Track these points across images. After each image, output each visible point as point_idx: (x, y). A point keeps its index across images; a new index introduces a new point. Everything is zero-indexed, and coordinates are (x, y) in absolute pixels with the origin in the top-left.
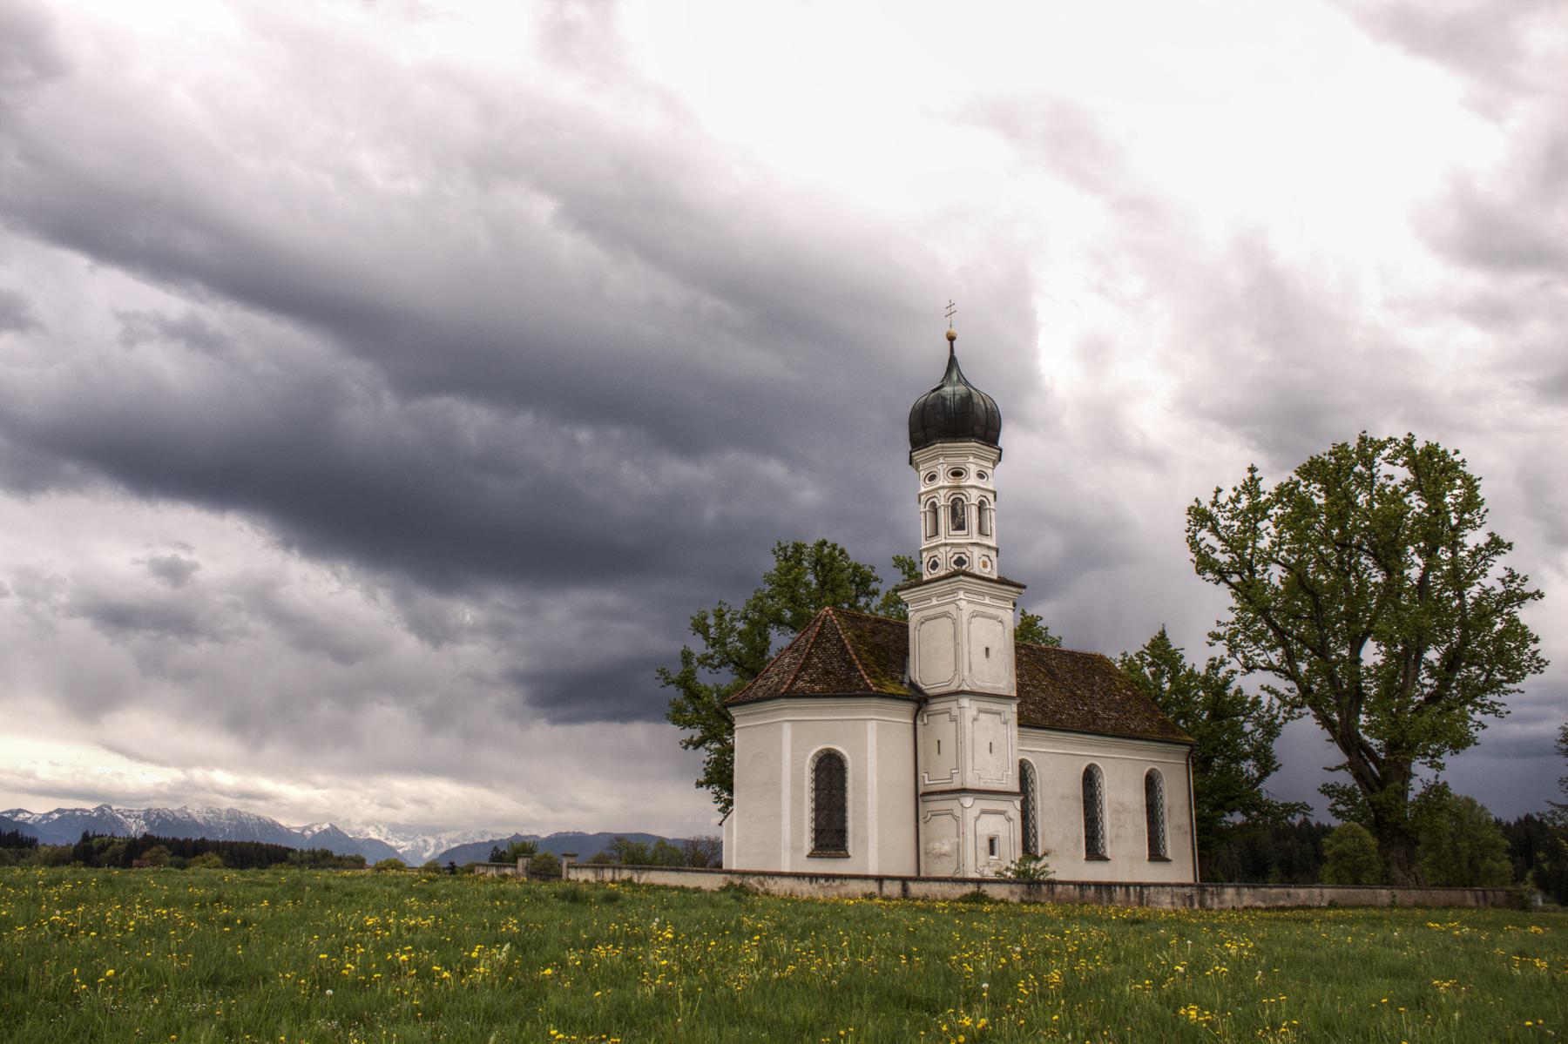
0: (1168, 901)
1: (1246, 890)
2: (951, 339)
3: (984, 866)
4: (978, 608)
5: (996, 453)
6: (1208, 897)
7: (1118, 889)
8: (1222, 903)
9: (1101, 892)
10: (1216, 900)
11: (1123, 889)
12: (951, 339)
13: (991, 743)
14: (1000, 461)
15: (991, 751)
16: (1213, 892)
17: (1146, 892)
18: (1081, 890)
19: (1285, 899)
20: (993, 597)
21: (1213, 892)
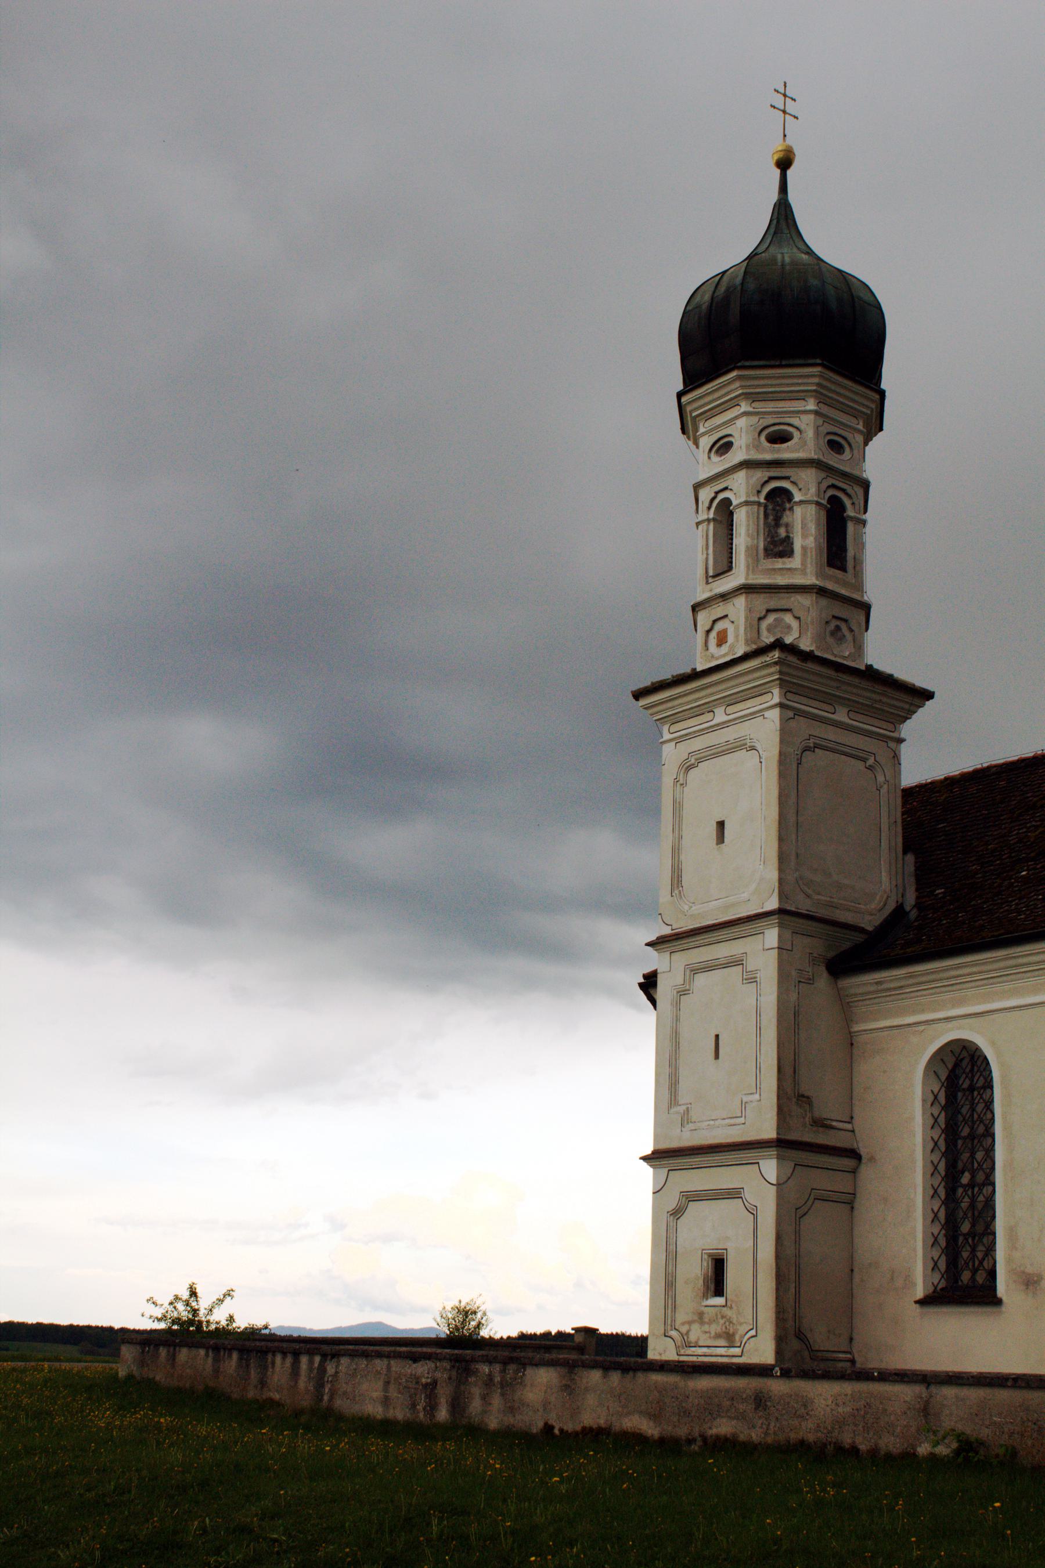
0: (375, 1395)
1: (595, 1376)
2: (784, 163)
3: (690, 1323)
4: (697, 744)
5: (873, 401)
6: (476, 1391)
7: (278, 1359)
8: (512, 1410)
9: (248, 1366)
10: (497, 1401)
11: (289, 1360)
12: (784, 163)
13: (717, 1036)
14: (881, 429)
15: (717, 1057)
16: (490, 1377)
17: (330, 1369)
18: (216, 1360)
19: (741, 1417)
20: (854, 708)
21: (490, 1377)
